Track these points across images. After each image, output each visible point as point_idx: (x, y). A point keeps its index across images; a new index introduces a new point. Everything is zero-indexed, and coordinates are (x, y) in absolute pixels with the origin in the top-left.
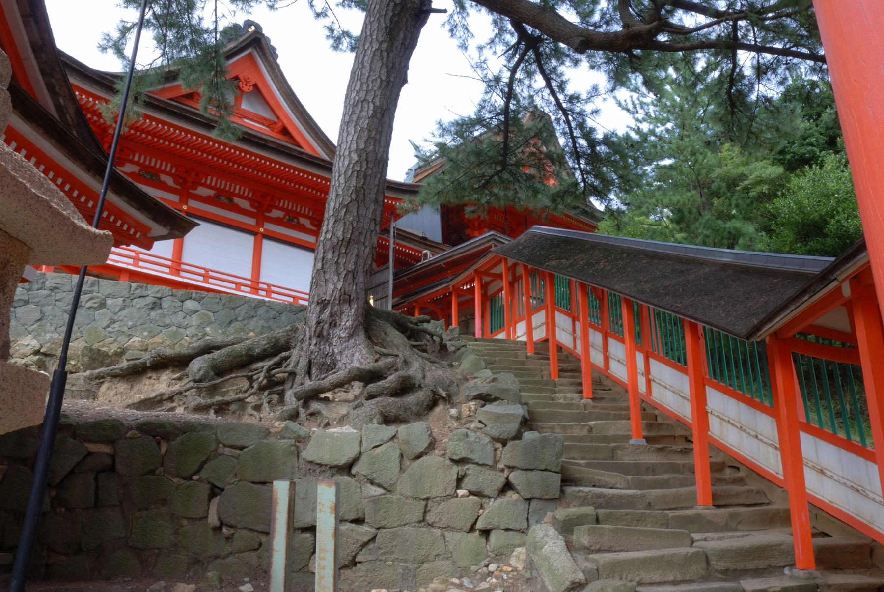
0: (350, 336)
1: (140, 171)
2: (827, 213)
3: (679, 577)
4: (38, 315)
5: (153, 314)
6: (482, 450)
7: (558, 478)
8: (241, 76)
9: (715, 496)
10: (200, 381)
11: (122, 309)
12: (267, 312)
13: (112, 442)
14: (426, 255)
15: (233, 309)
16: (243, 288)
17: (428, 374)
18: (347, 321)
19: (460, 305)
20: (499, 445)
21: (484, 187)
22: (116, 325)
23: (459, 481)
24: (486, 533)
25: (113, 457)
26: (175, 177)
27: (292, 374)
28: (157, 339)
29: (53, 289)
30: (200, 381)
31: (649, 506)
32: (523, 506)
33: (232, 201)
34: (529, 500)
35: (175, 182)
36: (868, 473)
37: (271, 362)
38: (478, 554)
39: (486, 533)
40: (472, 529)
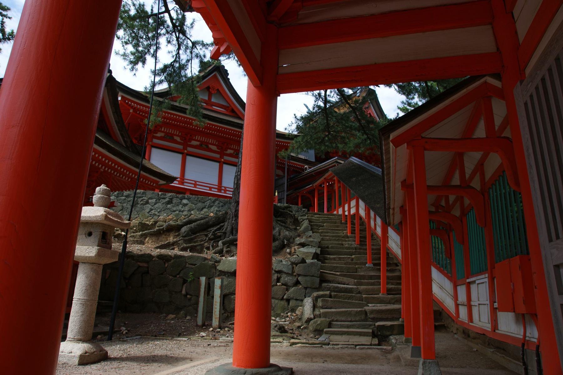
3: (353, 320)
4: (121, 208)
5: (169, 206)
7: (317, 280)
8: (211, 86)
10: (185, 236)
11: (155, 204)
12: (219, 203)
13: (147, 262)
14: (306, 168)
15: (204, 203)
16: (213, 189)
17: (282, 234)
19: (319, 195)
20: (294, 266)
21: (321, 142)
22: (153, 211)
24: (288, 301)
25: (148, 268)
26: (180, 137)
27: (225, 233)
28: (170, 217)
29: (126, 196)
30: (185, 236)
31: (359, 293)
33: (208, 146)
35: (181, 139)
37: (215, 228)
38: (284, 309)
39: (288, 301)
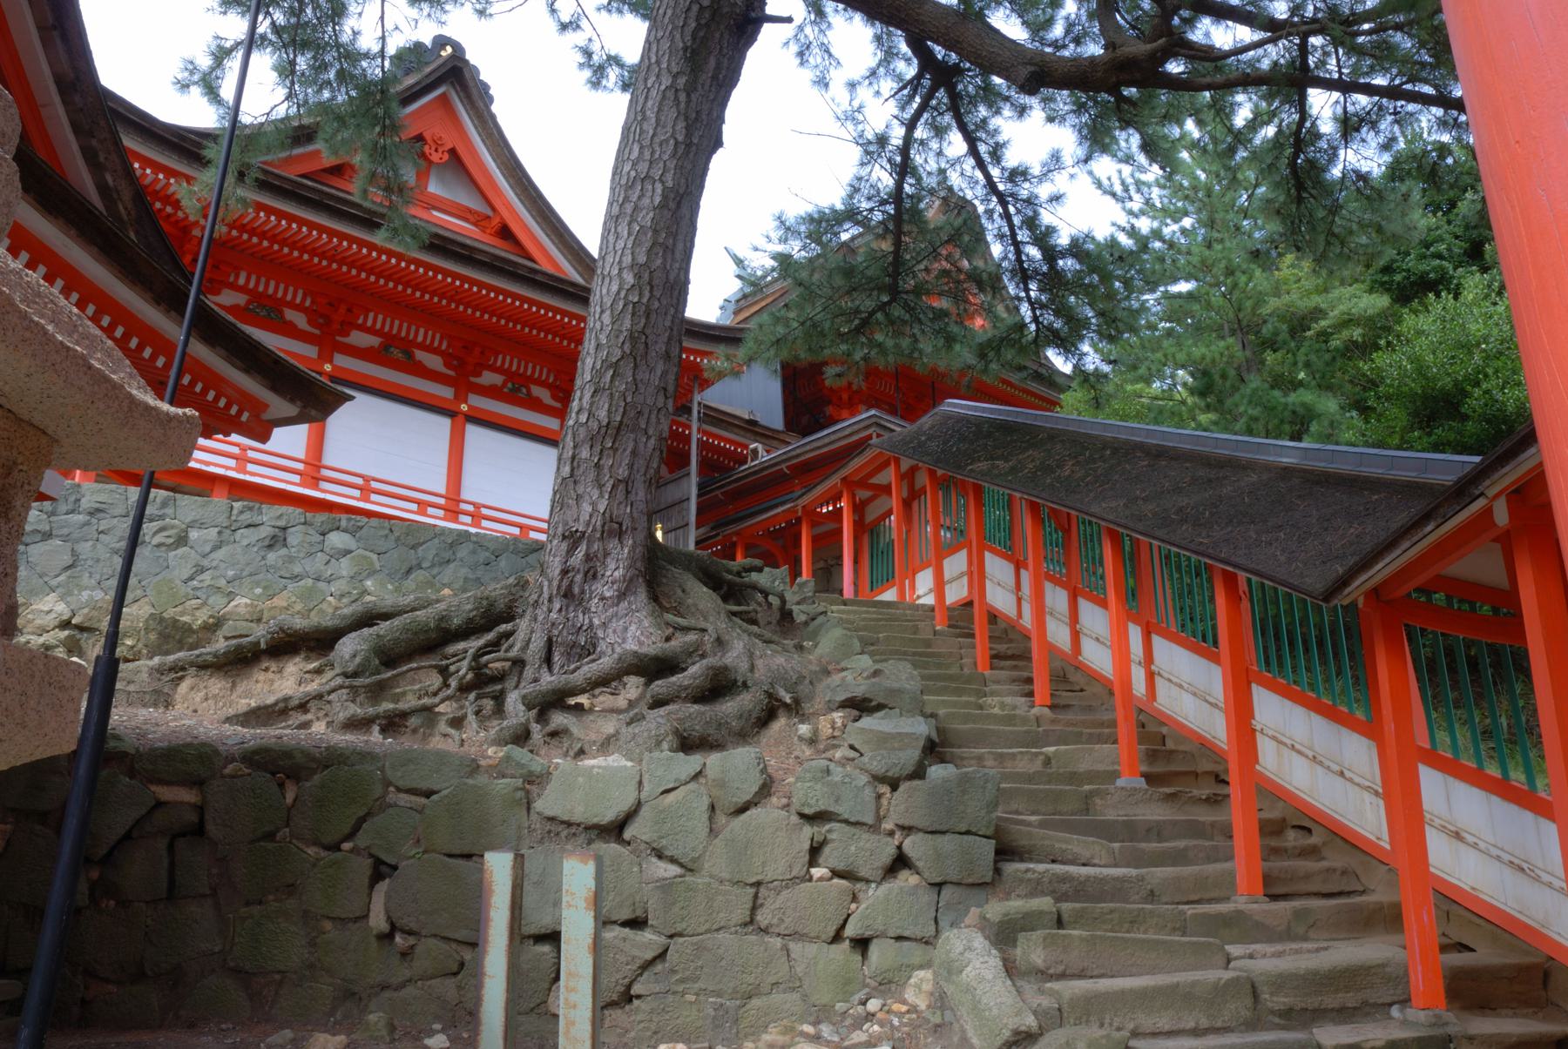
0: (622, 596)
1: (249, 302)
2: (1466, 378)
3: (1204, 1023)
4: (67, 559)
5: (272, 557)
6: (856, 798)
7: (989, 847)
8: (427, 135)
9: (1268, 880)
10: (355, 675)
11: (216, 548)
12: (474, 552)
13: (198, 783)
14: (755, 451)
15: (413, 547)
16: (431, 510)
17: (759, 663)
18: (615, 568)
19: (816, 540)
20: (885, 789)
21: (858, 331)
22: (206, 576)
23: (815, 852)
24: (862, 944)
25: (200, 809)
26: (311, 314)
27: (519, 663)
28: (279, 601)
29: (93, 513)
30: (355, 675)
31: (1152, 896)
32: (928, 897)
33: (411, 356)
34: (939, 886)
35: (310, 322)
36: (1540, 839)
37: (481, 642)
38: (848, 982)
39: (862, 944)
40: (837, 937)
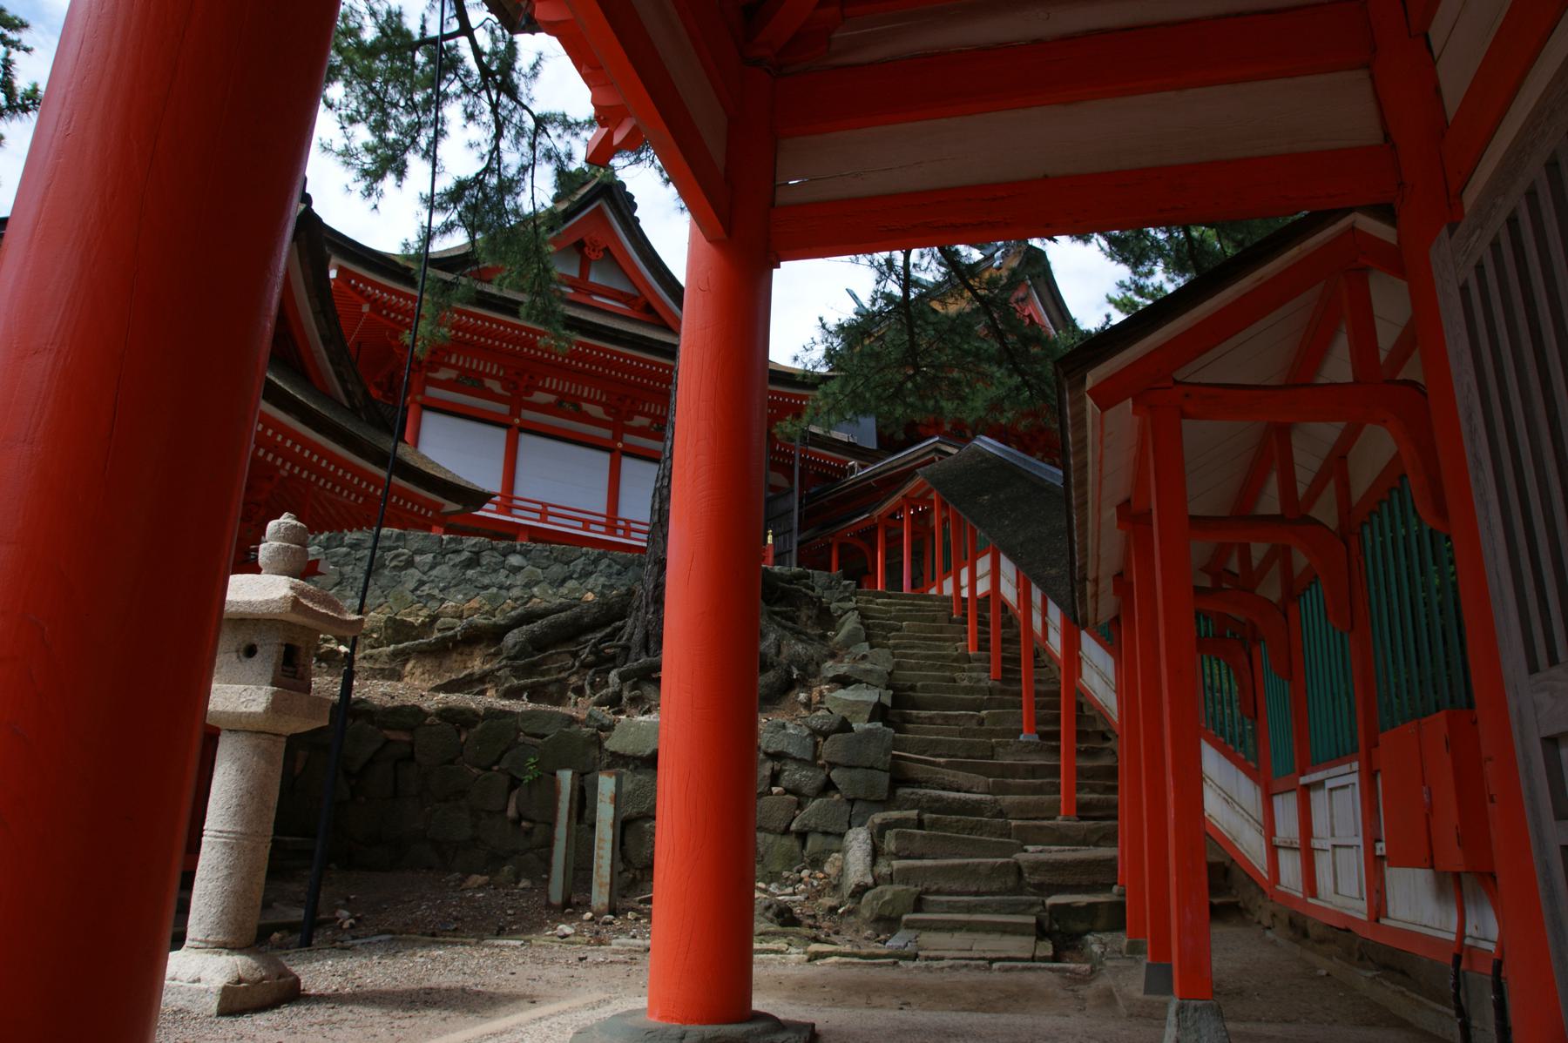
3: (983, 889)
4: (336, 578)
5: (470, 573)
7: (884, 779)
8: (586, 240)
10: (515, 658)
11: (432, 567)
12: (609, 566)
13: (411, 730)
14: (852, 467)
15: (568, 563)
16: (592, 527)
17: (785, 651)
19: (888, 541)
20: (820, 739)
21: (895, 395)
22: (426, 588)
24: (802, 836)
25: (411, 744)
26: (502, 380)
27: (626, 649)
28: (474, 604)
29: (352, 546)
30: (515, 658)
31: (1001, 814)
33: (579, 407)
35: (503, 387)
37: (599, 635)
38: (792, 859)
39: (802, 836)
